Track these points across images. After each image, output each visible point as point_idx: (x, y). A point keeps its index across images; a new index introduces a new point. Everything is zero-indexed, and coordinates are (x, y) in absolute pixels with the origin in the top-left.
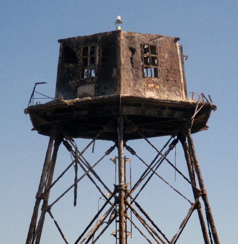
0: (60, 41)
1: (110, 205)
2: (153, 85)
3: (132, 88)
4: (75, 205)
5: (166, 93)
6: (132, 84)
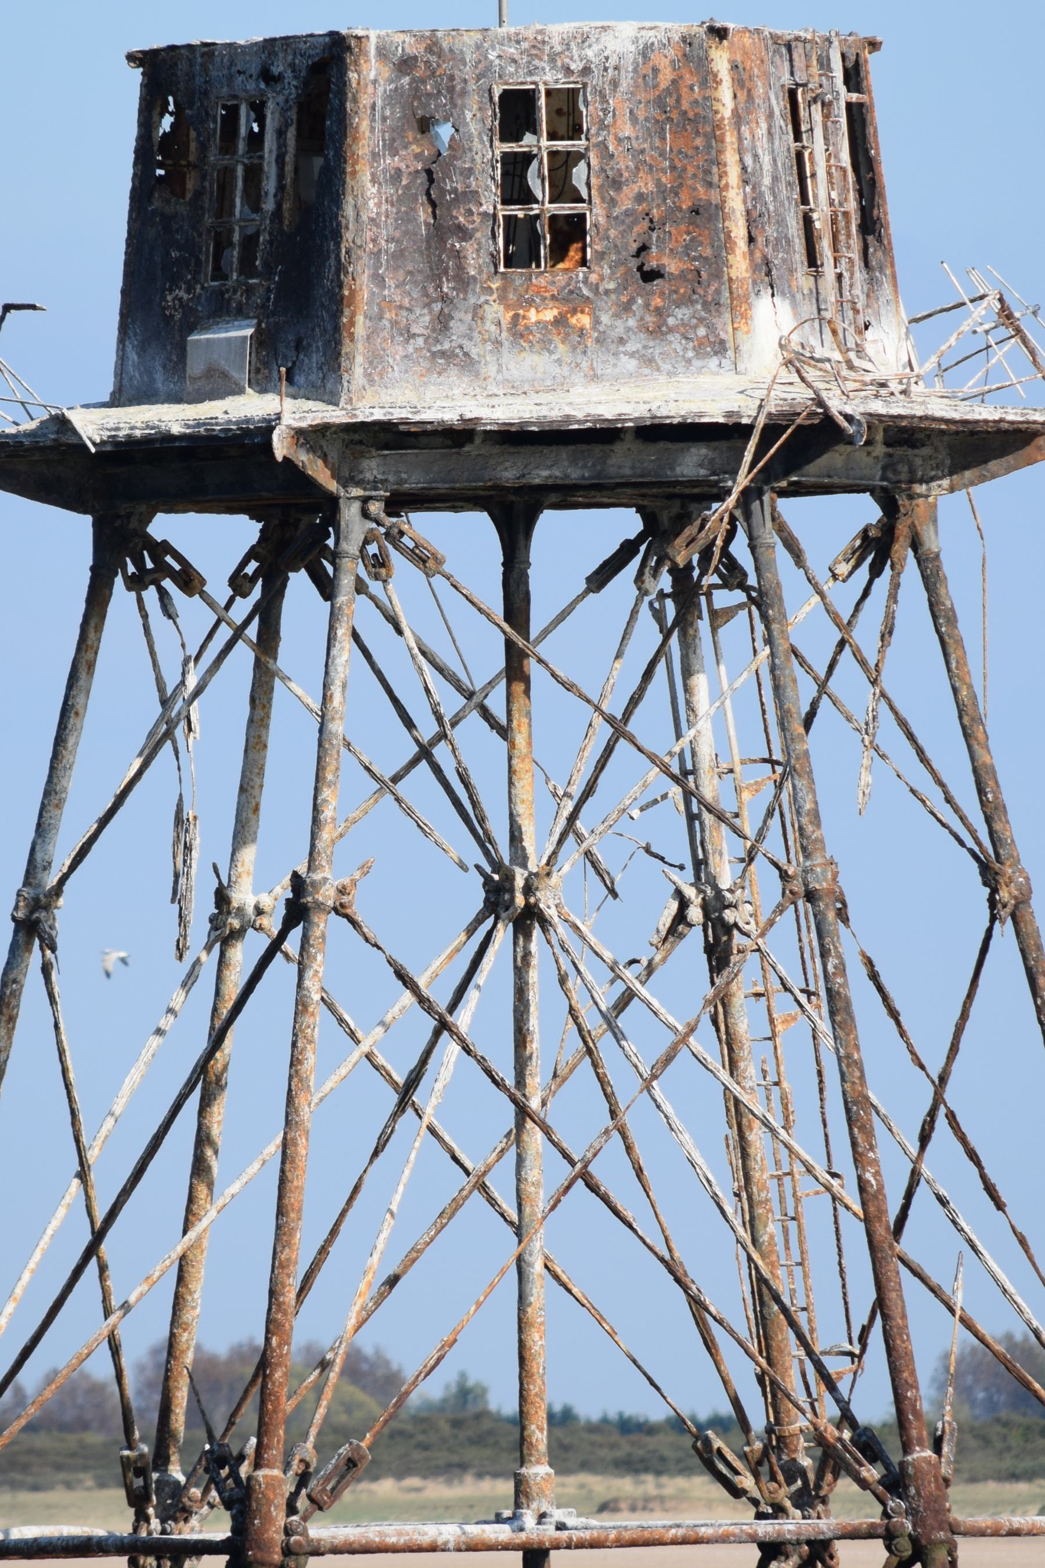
0: (140, 59)
1: (855, 1487)
2: (555, 312)
3: (420, 341)
5: (631, 346)
6: (422, 322)
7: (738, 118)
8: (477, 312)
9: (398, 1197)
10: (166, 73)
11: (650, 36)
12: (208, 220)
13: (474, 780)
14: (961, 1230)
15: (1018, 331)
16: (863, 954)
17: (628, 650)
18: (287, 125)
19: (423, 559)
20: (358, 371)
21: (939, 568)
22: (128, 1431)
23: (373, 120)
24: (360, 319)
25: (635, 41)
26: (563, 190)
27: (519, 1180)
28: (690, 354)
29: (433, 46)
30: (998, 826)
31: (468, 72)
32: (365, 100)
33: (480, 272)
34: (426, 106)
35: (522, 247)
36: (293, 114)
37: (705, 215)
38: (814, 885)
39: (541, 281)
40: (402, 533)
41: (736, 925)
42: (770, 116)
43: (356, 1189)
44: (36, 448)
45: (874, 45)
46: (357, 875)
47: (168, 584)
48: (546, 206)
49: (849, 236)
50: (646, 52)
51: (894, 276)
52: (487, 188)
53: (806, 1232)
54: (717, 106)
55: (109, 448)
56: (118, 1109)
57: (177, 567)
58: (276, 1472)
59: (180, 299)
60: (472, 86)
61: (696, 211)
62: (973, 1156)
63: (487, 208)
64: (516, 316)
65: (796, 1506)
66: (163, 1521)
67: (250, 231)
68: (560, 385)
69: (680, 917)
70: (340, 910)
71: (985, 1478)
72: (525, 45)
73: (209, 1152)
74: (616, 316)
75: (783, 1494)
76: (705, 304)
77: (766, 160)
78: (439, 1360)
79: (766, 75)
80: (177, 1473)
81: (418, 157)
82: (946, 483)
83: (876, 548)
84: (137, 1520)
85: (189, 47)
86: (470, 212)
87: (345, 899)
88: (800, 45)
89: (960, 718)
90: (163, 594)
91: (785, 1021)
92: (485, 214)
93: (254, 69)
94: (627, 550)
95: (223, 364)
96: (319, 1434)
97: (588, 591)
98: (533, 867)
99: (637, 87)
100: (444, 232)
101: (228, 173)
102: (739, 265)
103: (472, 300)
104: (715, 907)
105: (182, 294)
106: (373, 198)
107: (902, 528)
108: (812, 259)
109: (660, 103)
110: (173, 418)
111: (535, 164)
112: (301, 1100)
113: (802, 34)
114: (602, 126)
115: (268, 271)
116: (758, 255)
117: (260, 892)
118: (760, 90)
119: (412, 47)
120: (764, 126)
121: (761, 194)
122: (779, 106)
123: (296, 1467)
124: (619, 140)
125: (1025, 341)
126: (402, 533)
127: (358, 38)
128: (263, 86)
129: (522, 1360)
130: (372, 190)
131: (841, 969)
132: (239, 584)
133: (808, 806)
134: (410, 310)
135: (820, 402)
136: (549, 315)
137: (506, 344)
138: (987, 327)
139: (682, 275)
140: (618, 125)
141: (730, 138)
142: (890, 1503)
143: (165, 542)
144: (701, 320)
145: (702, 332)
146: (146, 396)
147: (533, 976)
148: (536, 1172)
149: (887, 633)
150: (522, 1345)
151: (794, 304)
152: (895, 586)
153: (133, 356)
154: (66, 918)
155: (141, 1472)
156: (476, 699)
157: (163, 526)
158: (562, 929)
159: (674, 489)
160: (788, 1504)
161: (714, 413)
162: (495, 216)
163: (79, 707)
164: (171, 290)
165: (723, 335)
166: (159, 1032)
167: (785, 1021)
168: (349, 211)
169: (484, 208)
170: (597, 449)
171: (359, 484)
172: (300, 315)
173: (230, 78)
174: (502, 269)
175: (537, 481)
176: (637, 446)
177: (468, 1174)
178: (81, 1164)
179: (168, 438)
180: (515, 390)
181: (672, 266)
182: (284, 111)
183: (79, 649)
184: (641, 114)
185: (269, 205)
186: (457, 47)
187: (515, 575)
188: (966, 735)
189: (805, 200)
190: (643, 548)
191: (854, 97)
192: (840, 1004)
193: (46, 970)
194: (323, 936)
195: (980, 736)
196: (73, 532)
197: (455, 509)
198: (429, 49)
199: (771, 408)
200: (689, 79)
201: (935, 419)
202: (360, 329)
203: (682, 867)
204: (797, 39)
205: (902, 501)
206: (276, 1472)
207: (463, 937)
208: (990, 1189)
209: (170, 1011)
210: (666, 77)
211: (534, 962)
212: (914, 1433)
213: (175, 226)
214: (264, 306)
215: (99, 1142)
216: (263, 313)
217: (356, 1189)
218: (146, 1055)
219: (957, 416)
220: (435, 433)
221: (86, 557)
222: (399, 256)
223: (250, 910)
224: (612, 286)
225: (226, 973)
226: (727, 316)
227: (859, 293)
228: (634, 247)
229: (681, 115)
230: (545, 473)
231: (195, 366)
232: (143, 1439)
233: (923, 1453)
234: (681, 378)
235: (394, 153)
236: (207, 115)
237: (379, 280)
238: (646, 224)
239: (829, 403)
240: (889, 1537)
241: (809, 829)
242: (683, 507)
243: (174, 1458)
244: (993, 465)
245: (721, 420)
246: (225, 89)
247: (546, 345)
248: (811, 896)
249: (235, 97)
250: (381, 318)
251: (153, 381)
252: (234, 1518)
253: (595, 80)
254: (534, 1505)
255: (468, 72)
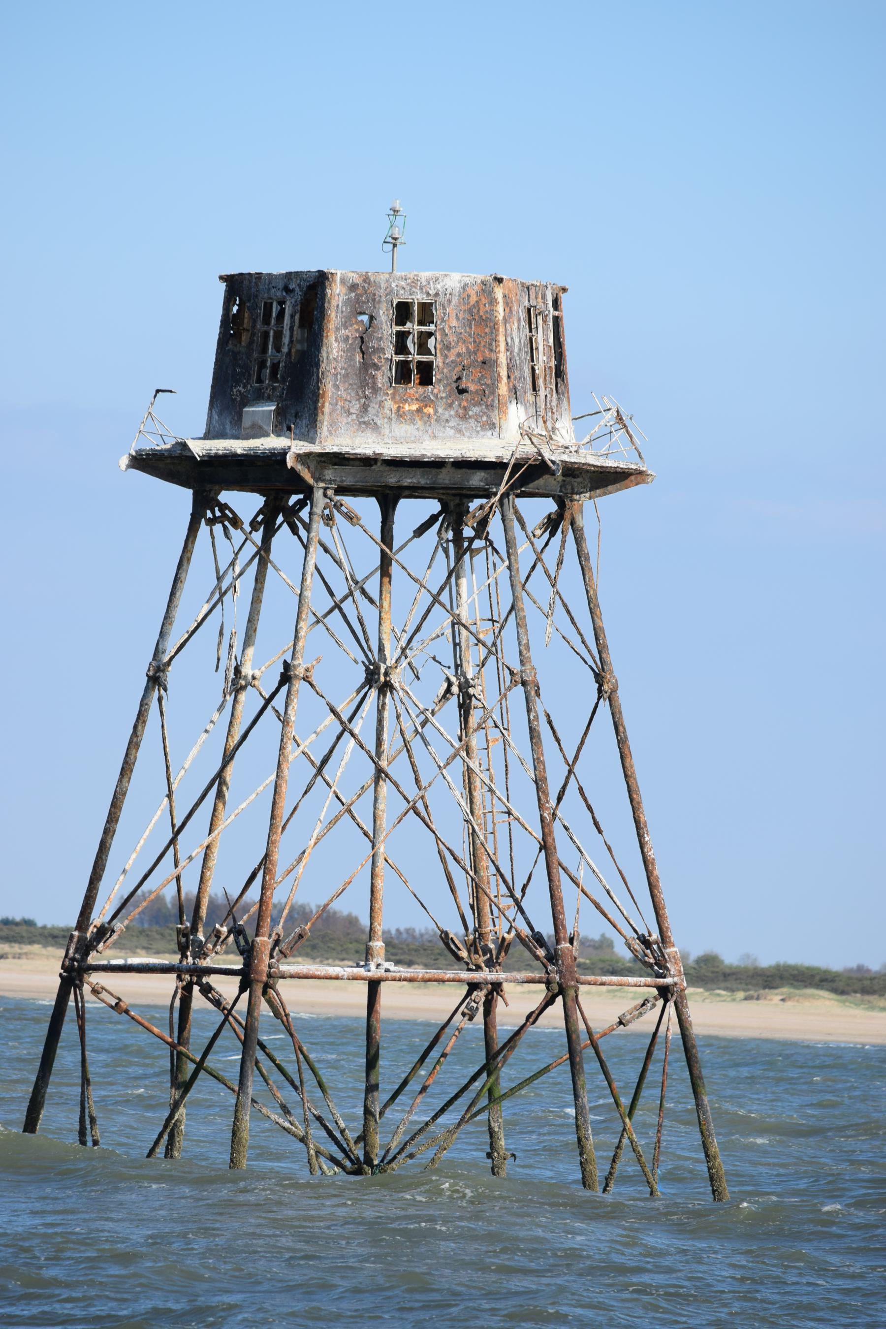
0: (225, 279)
2: (417, 406)
3: (354, 416)
4: (216, 671)
5: (451, 424)
6: (355, 407)
7: (505, 320)
8: (381, 404)
9: (323, 814)
10: (237, 286)
11: (467, 280)
12: (255, 355)
13: (365, 622)
14: (574, 842)
15: (625, 426)
16: (545, 712)
17: (433, 565)
18: (295, 313)
19: (351, 518)
20: (325, 429)
21: (582, 534)
22: (181, 917)
23: (337, 312)
24: (327, 404)
25: (460, 282)
26: (423, 348)
27: (375, 809)
28: (479, 429)
29: (366, 280)
30: (604, 655)
31: (382, 292)
32: (334, 303)
33: (383, 385)
34: (361, 307)
35: (403, 374)
36: (298, 308)
37: (488, 364)
38: (525, 678)
39: (412, 391)
40: (342, 505)
41: (474, 695)
42: (519, 320)
43: (295, 809)
44: (171, 457)
45: (564, 290)
46: (314, 663)
47: (226, 523)
48: (415, 357)
49: (551, 378)
50: (465, 287)
51: (568, 398)
52: (388, 347)
53: (497, 839)
54: (496, 314)
55: (206, 459)
56: (186, 766)
57: (231, 516)
58: (266, 939)
59: (240, 391)
60: (383, 299)
61: (484, 363)
62: (589, 808)
63: (388, 356)
64: (399, 407)
65: (487, 966)
66: (194, 959)
67: (275, 361)
68: (417, 440)
69: (448, 691)
70: (306, 679)
71: (164, 952)
72: (409, 281)
73: (224, 788)
74: (445, 409)
75: (481, 960)
76: (487, 406)
77: (516, 340)
78: (343, 890)
79: (518, 301)
80: (201, 936)
81: (357, 330)
82: (588, 495)
83: (552, 524)
84: (182, 957)
85: (250, 274)
86: (380, 358)
87: (308, 674)
88: (534, 288)
89: (589, 604)
90: (225, 528)
91: (493, 741)
92: (387, 359)
93: (281, 286)
94: (433, 519)
95: (260, 423)
96: (285, 922)
97: (414, 537)
98: (388, 663)
99: (460, 303)
100: (367, 366)
101: (266, 335)
102: (503, 388)
103: (379, 398)
104: (465, 686)
105: (241, 389)
106: (335, 349)
107: (567, 515)
108: (534, 388)
109: (470, 311)
110: (238, 446)
111: (411, 337)
112: (284, 766)
113: (535, 283)
114: (443, 321)
115: (284, 380)
116: (511, 384)
117: (261, 667)
118: (515, 308)
119: (357, 280)
120: (516, 324)
121: (514, 356)
122: (523, 315)
123: (274, 937)
124: (450, 328)
125: (627, 431)
126: (342, 505)
127: (332, 274)
128: (284, 294)
129: (372, 892)
130: (335, 345)
131: (537, 718)
132: (254, 525)
133: (524, 641)
134: (350, 402)
135: (540, 454)
136: (414, 407)
137: (394, 420)
138: (611, 423)
139: (477, 392)
140: (450, 322)
141: (501, 329)
142: (550, 968)
143: (226, 504)
144: (484, 413)
145: (485, 418)
146: (221, 435)
147: (386, 714)
148: (383, 805)
149: (560, 563)
150: (372, 885)
151: (526, 408)
152: (564, 541)
153: (216, 417)
154: (172, 676)
155: (186, 935)
156: (359, 585)
157: (225, 497)
158: (401, 693)
159: (458, 492)
160: (483, 965)
161: (491, 457)
162: (391, 360)
163: (182, 579)
164: (235, 387)
165: (494, 421)
166: (206, 731)
167: (493, 741)
168: (324, 354)
169: (386, 356)
170: (434, 471)
171: (323, 481)
172: (299, 401)
173: (269, 289)
174: (393, 385)
175: (406, 484)
176: (452, 470)
177: (343, 804)
178: (169, 791)
179: (235, 455)
180: (397, 441)
181: (472, 387)
182: (294, 306)
183: (183, 552)
184: (461, 317)
185: (285, 350)
186: (378, 280)
187: (387, 527)
188: (591, 613)
189: (532, 361)
190: (441, 518)
191: (557, 313)
192: (535, 734)
193: (160, 700)
194: (297, 691)
195: (598, 613)
196: (184, 497)
197: (354, 496)
198: (364, 281)
199: (517, 455)
200: (484, 301)
201: (589, 465)
202: (327, 408)
203: (449, 668)
204: (533, 285)
205: (567, 502)
206: (266, 939)
207: (355, 694)
208: (596, 824)
209: (212, 722)
210: (473, 299)
211: (387, 707)
212: (562, 935)
213: (239, 357)
214: (281, 396)
215: (177, 781)
216: (280, 399)
217: (295, 809)
218: (200, 741)
219: (599, 464)
220: (356, 459)
221: (189, 509)
222: (346, 376)
223: (250, 677)
224: (444, 395)
225: (237, 706)
226: (497, 412)
227: (554, 403)
228: (455, 377)
229: (480, 319)
230: (409, 481)
231: (246, 422)
232: (187, 920)
233: (565, 945)
234: (474, 439)
235: (346, 328)
236: (256, 306)
237: (337, 387)
238: (461, 367)
239: (544, 455)
240: (548, 983)
241: (524, 652)
242: (461, 500)
243: (201, 929)
244: (610, 488)
245: (494, 460)
246: (266, 295)
247: (412, 421)
248: (524, 683)
249: (271, 298)
250: (336, 405)
251: (224, 428)
252: (244, 959)
253: (440, 299)
254: (375, 960)
255: (382, 292)
